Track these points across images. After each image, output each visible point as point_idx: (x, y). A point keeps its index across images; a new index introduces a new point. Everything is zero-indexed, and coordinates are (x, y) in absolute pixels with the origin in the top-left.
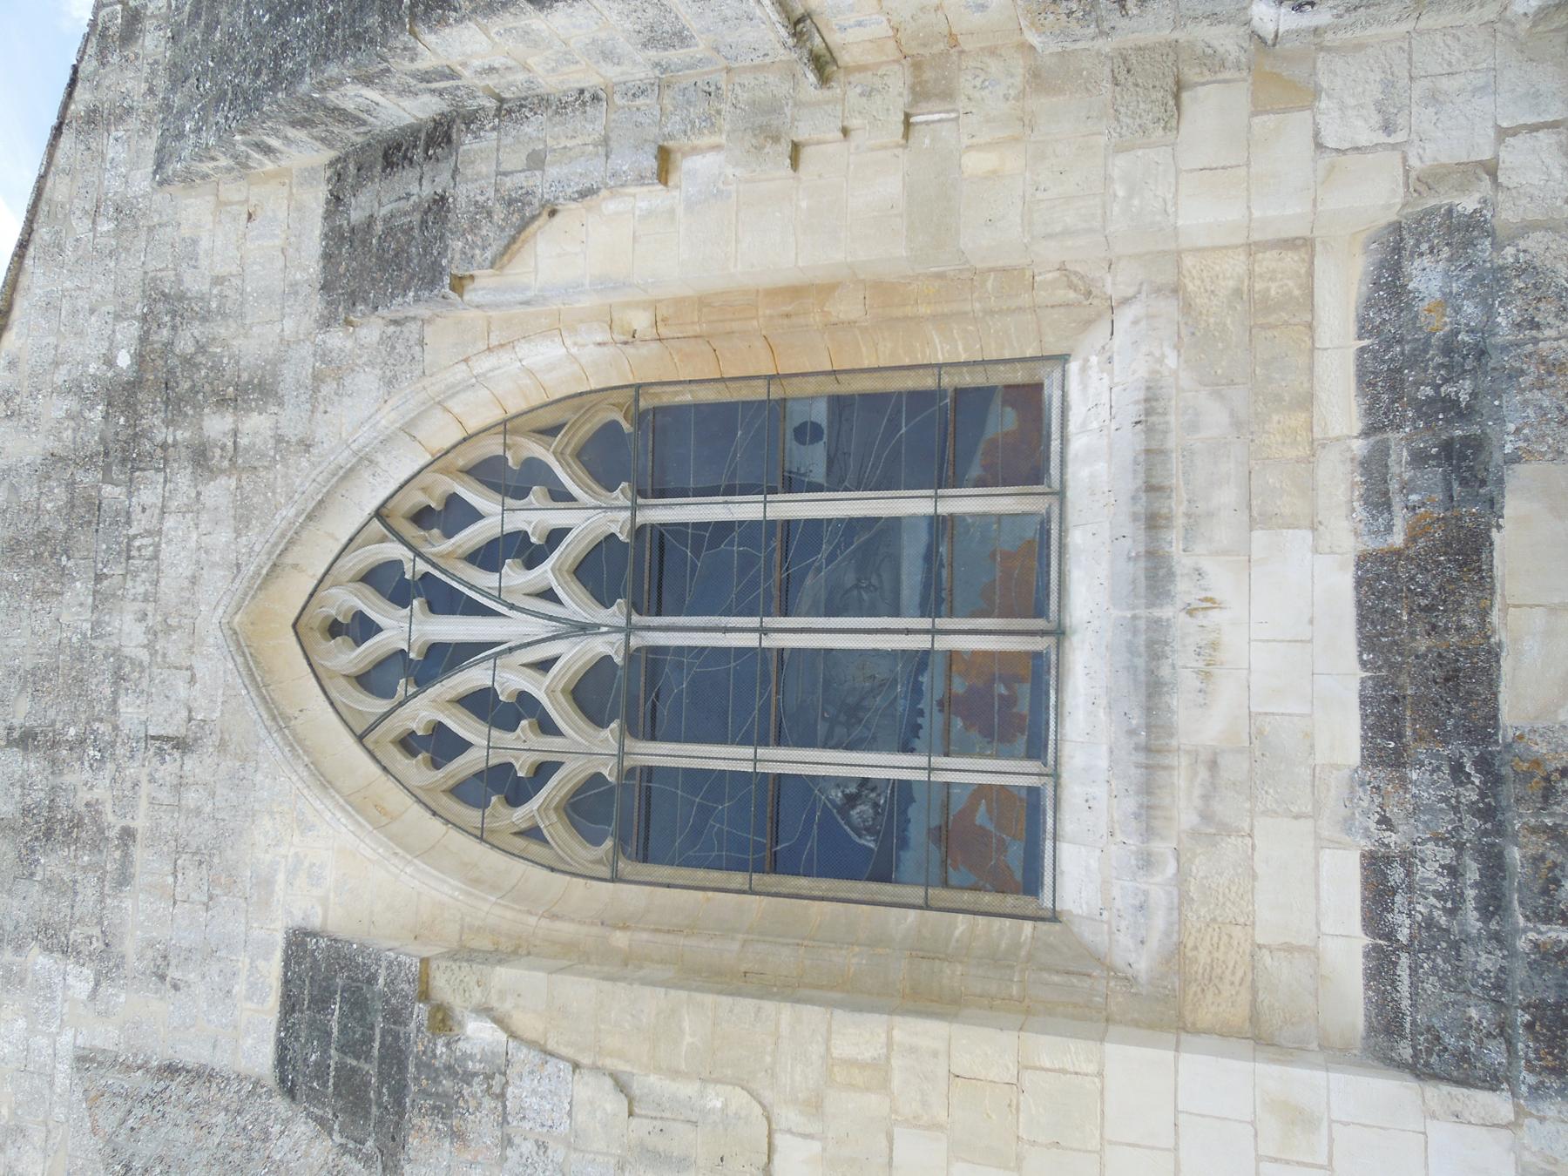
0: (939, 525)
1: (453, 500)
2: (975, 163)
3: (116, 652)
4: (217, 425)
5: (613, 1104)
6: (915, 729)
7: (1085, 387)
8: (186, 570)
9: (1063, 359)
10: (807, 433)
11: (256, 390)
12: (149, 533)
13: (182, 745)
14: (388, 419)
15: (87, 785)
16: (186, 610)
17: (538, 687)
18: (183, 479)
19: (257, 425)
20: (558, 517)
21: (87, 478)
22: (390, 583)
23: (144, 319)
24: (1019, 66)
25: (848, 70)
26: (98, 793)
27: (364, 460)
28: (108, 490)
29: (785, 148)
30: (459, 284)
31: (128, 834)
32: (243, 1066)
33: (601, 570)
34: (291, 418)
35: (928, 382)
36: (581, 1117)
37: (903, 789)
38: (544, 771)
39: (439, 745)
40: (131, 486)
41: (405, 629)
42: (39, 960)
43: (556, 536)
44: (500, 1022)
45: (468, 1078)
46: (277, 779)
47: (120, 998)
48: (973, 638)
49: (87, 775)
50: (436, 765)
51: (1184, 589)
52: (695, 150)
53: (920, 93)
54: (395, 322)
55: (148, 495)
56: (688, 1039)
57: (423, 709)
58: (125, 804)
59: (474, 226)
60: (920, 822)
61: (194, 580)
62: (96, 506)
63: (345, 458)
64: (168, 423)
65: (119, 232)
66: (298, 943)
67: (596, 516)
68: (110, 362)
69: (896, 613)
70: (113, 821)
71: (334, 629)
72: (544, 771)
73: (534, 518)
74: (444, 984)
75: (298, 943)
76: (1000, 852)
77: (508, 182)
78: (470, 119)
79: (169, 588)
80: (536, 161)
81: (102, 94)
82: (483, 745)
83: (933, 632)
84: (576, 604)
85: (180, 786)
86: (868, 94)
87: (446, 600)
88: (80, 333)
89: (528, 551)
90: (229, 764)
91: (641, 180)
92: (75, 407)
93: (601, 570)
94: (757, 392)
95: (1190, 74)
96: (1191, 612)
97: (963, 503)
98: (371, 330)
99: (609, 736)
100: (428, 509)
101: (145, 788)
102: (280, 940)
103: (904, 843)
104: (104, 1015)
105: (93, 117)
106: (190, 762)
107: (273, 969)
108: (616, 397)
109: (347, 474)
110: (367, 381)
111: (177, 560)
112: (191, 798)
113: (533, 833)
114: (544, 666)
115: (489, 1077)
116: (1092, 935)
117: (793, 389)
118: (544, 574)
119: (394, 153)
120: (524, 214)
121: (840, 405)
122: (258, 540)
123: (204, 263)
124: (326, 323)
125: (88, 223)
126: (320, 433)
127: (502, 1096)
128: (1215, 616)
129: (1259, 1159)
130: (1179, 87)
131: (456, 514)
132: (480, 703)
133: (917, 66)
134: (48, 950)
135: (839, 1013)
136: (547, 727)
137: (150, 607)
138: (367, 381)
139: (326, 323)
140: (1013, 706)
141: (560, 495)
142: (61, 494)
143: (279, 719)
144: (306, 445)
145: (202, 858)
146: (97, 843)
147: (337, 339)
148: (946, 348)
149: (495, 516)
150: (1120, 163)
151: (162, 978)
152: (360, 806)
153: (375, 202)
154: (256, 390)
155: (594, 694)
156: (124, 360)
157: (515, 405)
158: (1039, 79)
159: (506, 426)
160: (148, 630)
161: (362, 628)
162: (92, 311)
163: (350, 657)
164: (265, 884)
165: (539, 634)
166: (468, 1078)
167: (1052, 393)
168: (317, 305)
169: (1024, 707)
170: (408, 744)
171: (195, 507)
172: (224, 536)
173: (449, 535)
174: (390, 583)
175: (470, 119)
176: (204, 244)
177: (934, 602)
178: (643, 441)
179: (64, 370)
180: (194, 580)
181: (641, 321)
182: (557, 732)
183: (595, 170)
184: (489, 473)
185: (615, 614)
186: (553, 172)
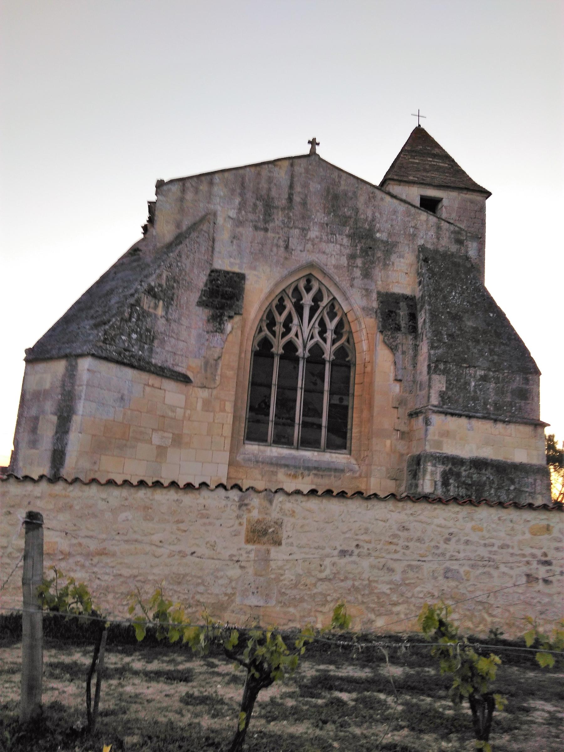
0: (320, 426)
1: (335, 315)
2: (388, 442)
3: (309, 229)
4: (359, 262)
5: (216, 356)
6: (279, 418)
7: (344, 458)
8: (327, 251)
9: (350, 454)
10: (341, 400)
11: (367, 275)
12: (336, 240)
13: (287, 247)
14: (356, 307)
15: (279, 217)
16: (318, 250)
17: (292, 334)
18: (348, 251)
19: (358, 273)
20: (329, 341)
21: (351, 222)
22: (317, 298)
23: (387, 242)
24: (405, 452)
25: (410, 420)
26: (277, 222)
27: (347, 299)
28: (348, 228)
29: (397, 406)
30: (381, 332)
31: (266, 230)
32: (215, 260)
33: (317, 351)
34: (358, 282)
35: (349, 427)
36: (213, 349)
37: (268, 414)
38: (274, 333)
39: (281, 307)
40: (348, 236)
41: (307, 300)
42: (237, 200)
43: (325, 340)
44: (231, 332)
45: (220, 324)
46: (277, 273)
47: (229, 225)
48: (297, 431)
49: (281, 219)
50: (276, 307)
51: (306, 472)
52: (400, 387)
53: (403, 433)
54: (376, 312)
55: (346, 241)
56: (228, 372)
57: (289, 306)
58: (274, 231)
59: (392, 338)
60: (261, 417)
61: (324, 253)
62: (344, 224)
63: (348, 294)
64: (361, 248)
65: (410, 235)
66: (242, 277)
67: (329, 351)
68: (378, 231)
69: (303, 415)
70: (271, 225)
71: (309, 281)
72: (274, 333)
73: (329, 335)
74: (237, 319)
75: (242, 277)
76: (255, 433)
77: (400, 346)
78: (416, 338)
79: (323, 246)
80: (404, 353)
81: (445, 231)
82: (281, 319)
83: (299, 424)
84: (310, 344)
85: (278, 246)
86: (405, 423)
87: (313, 310)
88: (386, 222)
89: (323, 332)
90: (282, 260)
91: (396, 376)
92: (369, 219)
93: (317, 351)
94: (351, 391)
95: (398, 482)
96: (302, 473)
97: (324, 432)
98: (375, 305)
99: (281, 351)
100: (334, 308)
101: (277, 236)
102: (242, 271)
103: (257, 414)
104: (225, 220)
105: (439, 228)
106: (282, 249)
107: (236, 269)
108: (354, 360)
109: (344, 294)
110: (364, 303)
111: (331, 248)
112: (275, 249)
113: (261, 330)
114: (297, 335)
115: (220, 329)
116: (242, 450)
117: (351, 398)
118: (317, 338)
119: (413, 317)
120: (393, 349)
121: (346, 407)
122: (331, 271)
123: (398, 260)
124: (379, 293)
125: (413, 225)
126: (354, 290)
127: (216, 331)
128: (301, 478)
129: (55, 478)
130: (395, 480)
131: (332, 315)
132: (289, 319)
133: (408, 433)
134: (240, 204)
135: (233, 404)
136: (284, 335)
137: (318, 240)
138: (364, 303)
139: (379, 293)
140: (282, 439)
141: (334, 342)
142: (348, 214)
143: (291, 274)
144: (352, 286)
145: (261, 251)
146: (266, 221)
147: (374, 296)
148: (355, 431)
149: (331, 325)
150: (384, 469)
151: (234, 238)
152: (270, 293)
153: (403, 312)
154: (367, 275)
155: (290, 347)
156: (378, 235)
157: (355, 335)
158: (402, 455)
159: (350, 332)
160: (314, 239)
161: (308, 289)
162: (392, 226)
163: (302, 285)
164: (255, 268)
165: (304, 333)
166: (220, 324)
167: (344, 451)
168: (383, 291)
169: (283, 440)
170: (281, 300)
171: (341, 254)
172: (334, 262)
173: (328, 313)
174: (317, 298)
175: (416, 338)
176: (402, 260)
177: (305, 425)
178: (344, 361)
179: (379, 216)
180: (324, 253)
181: (368, 369)
182: (282, 337)
183: (399, 366)
184: (340, 325)
185: (307, 354)
186: (401, 356)
